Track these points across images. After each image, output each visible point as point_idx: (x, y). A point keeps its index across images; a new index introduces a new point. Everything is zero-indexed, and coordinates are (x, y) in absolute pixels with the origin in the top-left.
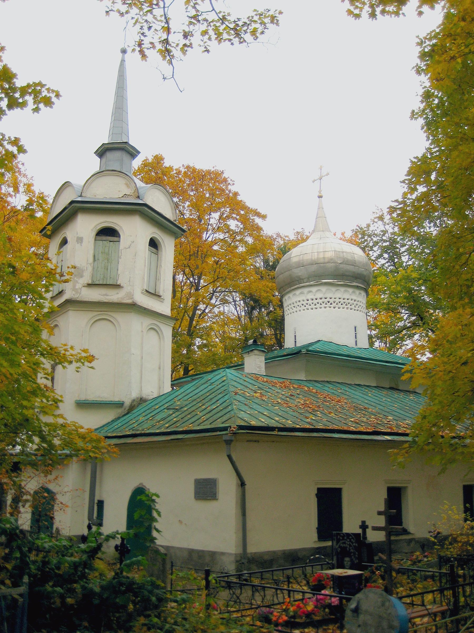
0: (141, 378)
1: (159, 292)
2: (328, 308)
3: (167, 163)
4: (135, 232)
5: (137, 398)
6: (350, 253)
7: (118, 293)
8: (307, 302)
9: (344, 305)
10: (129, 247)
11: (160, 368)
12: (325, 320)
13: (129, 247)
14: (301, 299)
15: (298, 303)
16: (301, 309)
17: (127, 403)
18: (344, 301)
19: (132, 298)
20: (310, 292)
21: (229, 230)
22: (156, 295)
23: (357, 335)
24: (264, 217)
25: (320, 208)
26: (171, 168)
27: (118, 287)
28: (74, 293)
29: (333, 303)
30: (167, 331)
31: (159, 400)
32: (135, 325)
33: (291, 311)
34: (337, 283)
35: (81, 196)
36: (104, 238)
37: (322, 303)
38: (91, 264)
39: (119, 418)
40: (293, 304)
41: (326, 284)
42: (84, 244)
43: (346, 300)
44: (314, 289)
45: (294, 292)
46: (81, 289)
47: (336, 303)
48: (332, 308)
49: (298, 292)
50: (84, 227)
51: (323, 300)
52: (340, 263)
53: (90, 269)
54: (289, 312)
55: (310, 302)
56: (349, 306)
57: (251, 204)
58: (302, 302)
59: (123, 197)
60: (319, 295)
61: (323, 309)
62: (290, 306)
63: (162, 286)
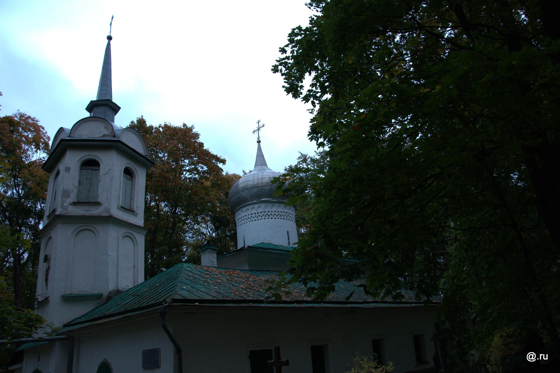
0: (118, 274)
2: (267, 219)
3: (148, 124)
4: (112, 164)
5: (114, 291)
9: (279, 216)
11: (134, 267)
12: (267, 228)
14: (247, 214)
17: (105, 294)
20: (254, 208)
21: (198, 173)
22: (131, 211)
23: (290, 238)
24: (223, 162)
25: (259, 149)
26: (151, 127)
27: (98, 204)
30: (141, 240)
31: (131, 290)
32: (113, 233)
33: (241, 223)
35: (70, 136)
36: (88, 168)
38: (76, 187)
39: (98, 307)
41: (264, 202)
42: (71, 172)
44: (256, 206)
46: (68, 207)
49: (244, 209)
50: (72, 160)
51: (263, 213)
53: (76, 191)
56: (282, 217)
57: (213, 151)
58: (248, 216)
60: (260, 210)
61: (263, 220)
63: (135, 204)
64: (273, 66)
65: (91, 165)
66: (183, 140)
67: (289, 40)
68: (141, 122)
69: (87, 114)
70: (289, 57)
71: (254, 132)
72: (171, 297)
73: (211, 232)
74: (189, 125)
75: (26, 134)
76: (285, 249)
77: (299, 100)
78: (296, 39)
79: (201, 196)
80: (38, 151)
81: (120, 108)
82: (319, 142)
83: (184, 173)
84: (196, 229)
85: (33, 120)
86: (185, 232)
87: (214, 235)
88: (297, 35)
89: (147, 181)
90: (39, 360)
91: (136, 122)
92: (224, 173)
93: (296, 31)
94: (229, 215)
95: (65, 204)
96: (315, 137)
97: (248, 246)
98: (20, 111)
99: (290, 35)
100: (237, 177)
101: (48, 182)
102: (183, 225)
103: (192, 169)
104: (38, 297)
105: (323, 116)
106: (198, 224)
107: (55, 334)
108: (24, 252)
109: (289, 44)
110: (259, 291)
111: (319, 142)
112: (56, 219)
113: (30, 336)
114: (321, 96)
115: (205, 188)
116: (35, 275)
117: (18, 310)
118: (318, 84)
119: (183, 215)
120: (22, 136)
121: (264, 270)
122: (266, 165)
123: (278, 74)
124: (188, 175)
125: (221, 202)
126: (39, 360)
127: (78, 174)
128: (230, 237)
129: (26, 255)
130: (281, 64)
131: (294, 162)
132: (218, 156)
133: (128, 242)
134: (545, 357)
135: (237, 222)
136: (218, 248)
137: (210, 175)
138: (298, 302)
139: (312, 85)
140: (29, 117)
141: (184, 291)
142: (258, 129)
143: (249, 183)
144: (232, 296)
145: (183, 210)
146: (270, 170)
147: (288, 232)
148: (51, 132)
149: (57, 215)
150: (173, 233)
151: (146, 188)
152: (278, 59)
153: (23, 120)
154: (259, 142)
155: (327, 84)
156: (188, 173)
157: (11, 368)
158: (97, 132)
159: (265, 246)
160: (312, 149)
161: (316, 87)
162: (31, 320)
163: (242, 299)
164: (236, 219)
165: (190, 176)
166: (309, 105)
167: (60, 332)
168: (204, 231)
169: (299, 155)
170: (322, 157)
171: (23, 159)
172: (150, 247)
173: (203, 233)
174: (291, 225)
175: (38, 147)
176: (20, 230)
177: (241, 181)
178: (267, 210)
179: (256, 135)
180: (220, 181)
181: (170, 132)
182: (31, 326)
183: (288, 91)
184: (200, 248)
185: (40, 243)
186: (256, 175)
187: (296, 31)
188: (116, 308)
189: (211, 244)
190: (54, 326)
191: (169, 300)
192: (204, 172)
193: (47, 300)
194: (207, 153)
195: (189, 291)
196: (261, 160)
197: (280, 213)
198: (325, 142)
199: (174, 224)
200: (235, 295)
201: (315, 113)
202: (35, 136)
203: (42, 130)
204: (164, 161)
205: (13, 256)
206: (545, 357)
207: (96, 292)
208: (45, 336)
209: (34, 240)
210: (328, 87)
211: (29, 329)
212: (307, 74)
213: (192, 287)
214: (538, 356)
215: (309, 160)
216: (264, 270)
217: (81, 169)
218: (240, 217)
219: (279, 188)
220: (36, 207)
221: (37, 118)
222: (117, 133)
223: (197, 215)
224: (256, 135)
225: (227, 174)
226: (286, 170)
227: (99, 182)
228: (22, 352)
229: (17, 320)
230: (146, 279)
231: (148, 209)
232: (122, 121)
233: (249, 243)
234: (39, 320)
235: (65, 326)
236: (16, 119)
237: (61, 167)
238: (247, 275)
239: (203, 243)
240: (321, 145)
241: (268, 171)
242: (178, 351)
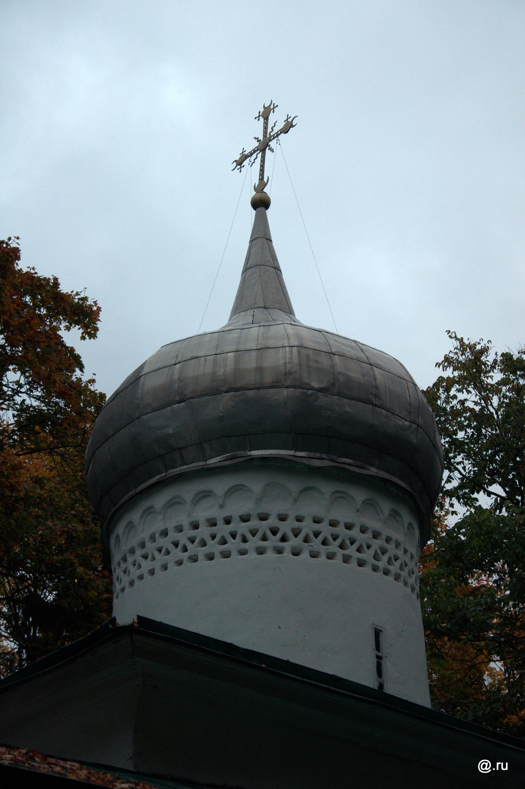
2: (270, 555)
6: (358, 360)
9: (334, 547)
14: (170, 525)
15: (161, 542)
16: (170, 559)
23: (387, 664)
25: (261, 236)
29: (290, 535)
34: (306, 461)
37: (249, 536)
40: (143, 545)
41: (265, 464)
43: (340, 529)
44: (219, 486)
45: (145, 504)
47: (302, 536)
48: (287, 554)
49: (159, 501)
51: (254, 523)
52: (321, 390)
55: (204, 531)
56: (351, 550)
60: (238, 507)
61: (252, 555)
62: (130, 559)
71: (240, 163)
122: (289, 310)
134: (504, 767)
135: (118, 572)
142: (263, 146)
143: (193, 370)
147: (377, 633)
154: (261, 203)
164: (116, 557)
178: (274, 508)
179: (251, 172)
186: (234, 335)
196: (262, 280)
197: (340, 529)
206: (504, 767)
218: (134, 541)
224: (251, 172)
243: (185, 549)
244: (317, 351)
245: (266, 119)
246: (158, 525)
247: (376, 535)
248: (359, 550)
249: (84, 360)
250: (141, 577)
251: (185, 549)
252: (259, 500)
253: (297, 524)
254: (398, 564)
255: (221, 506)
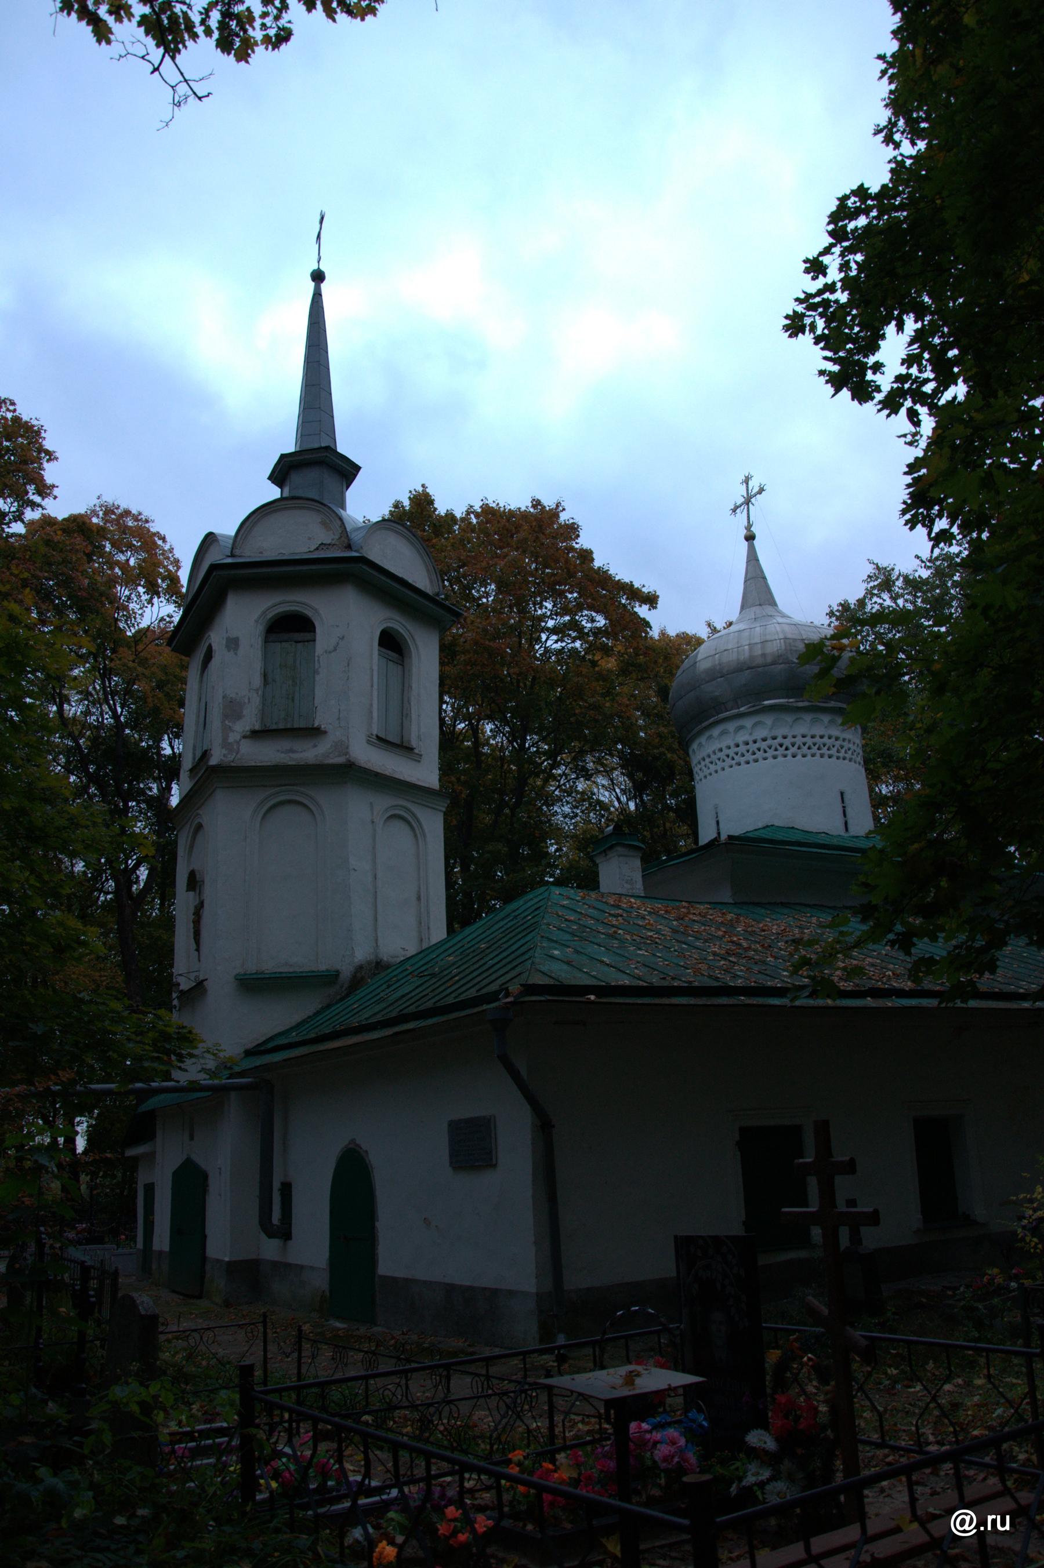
1: (409, 741)
2: (780, 759)
4: (349, 624)
5: (369, 963)
7: (315, 746)
8: (736, 749)
9: (814, 749)
10: (335, 649)
11: (419, 899)
12: (775, 783)
13: (335, 649)
14: (723, 745)
15: (719, 755)
16: (726, 765)
17: (346, 971)
18: (814, 740)
19: (347, 753)
22: (404, 748)
23: (849, 810)
24: (651, 600)
25: (752, 558)
26: (450, 516)
27: (315, 732)
28: (224, 751)
30: (433, 824)
32: (358, 811)
33: (706, 772)
34: (794, 705)
35: (232, 555)
38: (257, 690)
39: (328, 1006)
40: (709, 756)
41: (772, 708)
43: (817, 739)
44: (748, 722)
45: (707, 734)
46: (238, 743)
47: (796, 746)
48: (789, 757)
49: (716, 732)
50: (242, 618)
51: (769, 742)
53: (256, 700)
54: (702, 775)
55: (742, 748)
56: (824, 750)
57: (621, 572)
58: (726, 751)
59: (317, 549)
60: (760, 733)
61: (770, 760)
62: (703, 763)
64: (787, 317)
65: (291, 628)
66: (532, 546)
67: (831, 234)
68: (422, 501)
69: (274, 493)
70: (834, 283)
71: (734, 510)
72: (522, 979)
73: (624, 799)
74: (549, 502)
75: (122, 558)
76: (835, 842)
77: (870, 407)
78: (851, 226)
79: (591, 700)
80: (155, 600)
81: (357, 468)
82: (936, 529)
83: (544, 637)
84: (583, 793)
85: (136, 518)
86: (551, 800)
87: (632, 806)
88: (854, 214)
89: (442, 664)
90: (192, 1138)
91: (406, 503)
92: (655, 633)
93: (850, 203)
94: (670, 749)
95: (233, 737)
96: (924, 518)
97: (730, 837)
98: (104, 498)
99: (834, 218)
100: (690, 642)
101: (184, 681)
102: (546, 781)
103: (565, 624)
104: (181, 980)
105: (947, 451)
106: (588, 777)
107: (227, 1072)
108: (137, 866)
109: (832, 246)
110: (764, 962)
111: (936, 529)
112: (210, 777)
113: (167, 1076)
114: (937, 392)
115: (603, 677)
116: (168, 923)
117: (135, 1012)
118: (926, 356)
119: (545, 753)
120: (112, 564)
121: (775, 904)
122: (773, 603)
123: (806, 339)
124: (552, 643)
125: (646, 714)
126: (192, 1138)
127: (259, 654)
128: (677, 810)
129: (143, 873)
130: (812, 307)
131: (854, 593)
132: (636, 585)
133: (400, 832)
134: (1003, 1524)
135: (696, 770)
136: (643, 842)
137: (616, 639)
138: (876, 993)
139: (909, 361)
140: (127, 513)
141: (554, 963)
142: (748, 501)
144: (689, 977)
145: (543, 739)
146: (784, 616)
147: (842, 794)
148: (183, 549)
149: (213, 767)
150: (518, 804)
151: (442, 684)
152: (802, 296)
153: (111, 522)
154: (750, 538)
155: (953, 353)
156: (555, 637)
157: (130, 1152)
158: (300, 538)
159: (779, 836)
160: (911, 551)
161: (920, 365)
162: (166, 1037)
163: (716, 984)
164: (694, 762)
165: (558, 646)
166: (901, 422)
167: (237, 1069)
168: (605, 796)
169: (870, 569)
170: (939, 573)
171: (121, 625)
172: (457, 847)
173: (599, 802)
174: (849, 774)
175: (153, 590)
176: (127, 808)
177: (702, 651)
178: (780, 732)
179: (741, 517)
180: (645, 654)
181: (494, 521)
182: (168, 1053)
183: (837, 382)
184: (593, 845)
185: (176, 842)
186: (746, 634)
187: (850, 203)
188: (376, 1010)
189: (625, 832)
190: (222, 1054)
191: (514, 988)
192: (597, 632)
193: (200, 986)
194: (603, 578)
195: (568, 963)
196: (757, 589)
197: (817, 739)
198: (955, 530)
199: (522, 780)
200: (697, 972)
201: (923, 443)
202: (144, 560)
203: (160, 542)
204: (486, 606)
205: (114, 878)
206: (1003, 1524)
207: (323, 967)
208: (203, 1079)
209: (159, 834)
210: (956, 361)
211: (165, 1058)
212: (891, 329)
213: (577, 952)
214: (982, 1522)
215: (899, 583)
216: (775, 904)
217: (266, 641)
218: (704, 754)
219: (824, 672)
220: (159, 749)
221: (146, 513)
222: (356, 537)
223: (582, 753)
224: (741, 517)
225: (663, 634)
226: (831, 614)
227: (316, 672)
228: (151, 1115)
229: (133, 1037)
230: (450, 930)
231: (448, 739)
232: (366, 503)
233: (732, 827)
234: (187, 1037)
235: (249, 1053)
236: (95, 520)
237: (216, 638)
238: (729, 917)
239: (601, 830)
240: (944, 537)
241: (780, 620)
242: (544, 1126)
243: (733, 759)
244: (795, 640)
245: (747, 484)
246: (716, 746)
247: (837, 739)
248: (828, 749)
249: (652, 624)
250: (710, 774)
251: (733, 759)
252: (771, 729)
253: (793, 740)
254: (850, 752)
255: (751, 734)
